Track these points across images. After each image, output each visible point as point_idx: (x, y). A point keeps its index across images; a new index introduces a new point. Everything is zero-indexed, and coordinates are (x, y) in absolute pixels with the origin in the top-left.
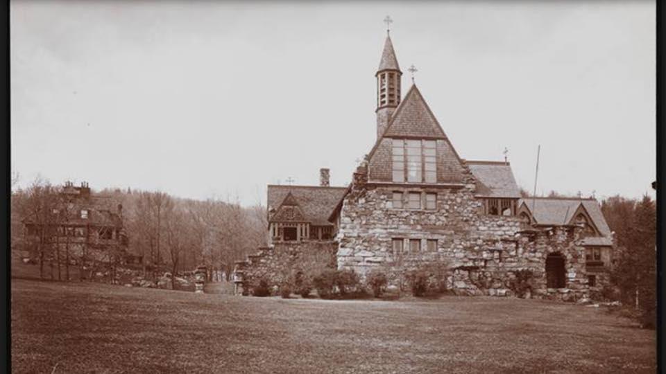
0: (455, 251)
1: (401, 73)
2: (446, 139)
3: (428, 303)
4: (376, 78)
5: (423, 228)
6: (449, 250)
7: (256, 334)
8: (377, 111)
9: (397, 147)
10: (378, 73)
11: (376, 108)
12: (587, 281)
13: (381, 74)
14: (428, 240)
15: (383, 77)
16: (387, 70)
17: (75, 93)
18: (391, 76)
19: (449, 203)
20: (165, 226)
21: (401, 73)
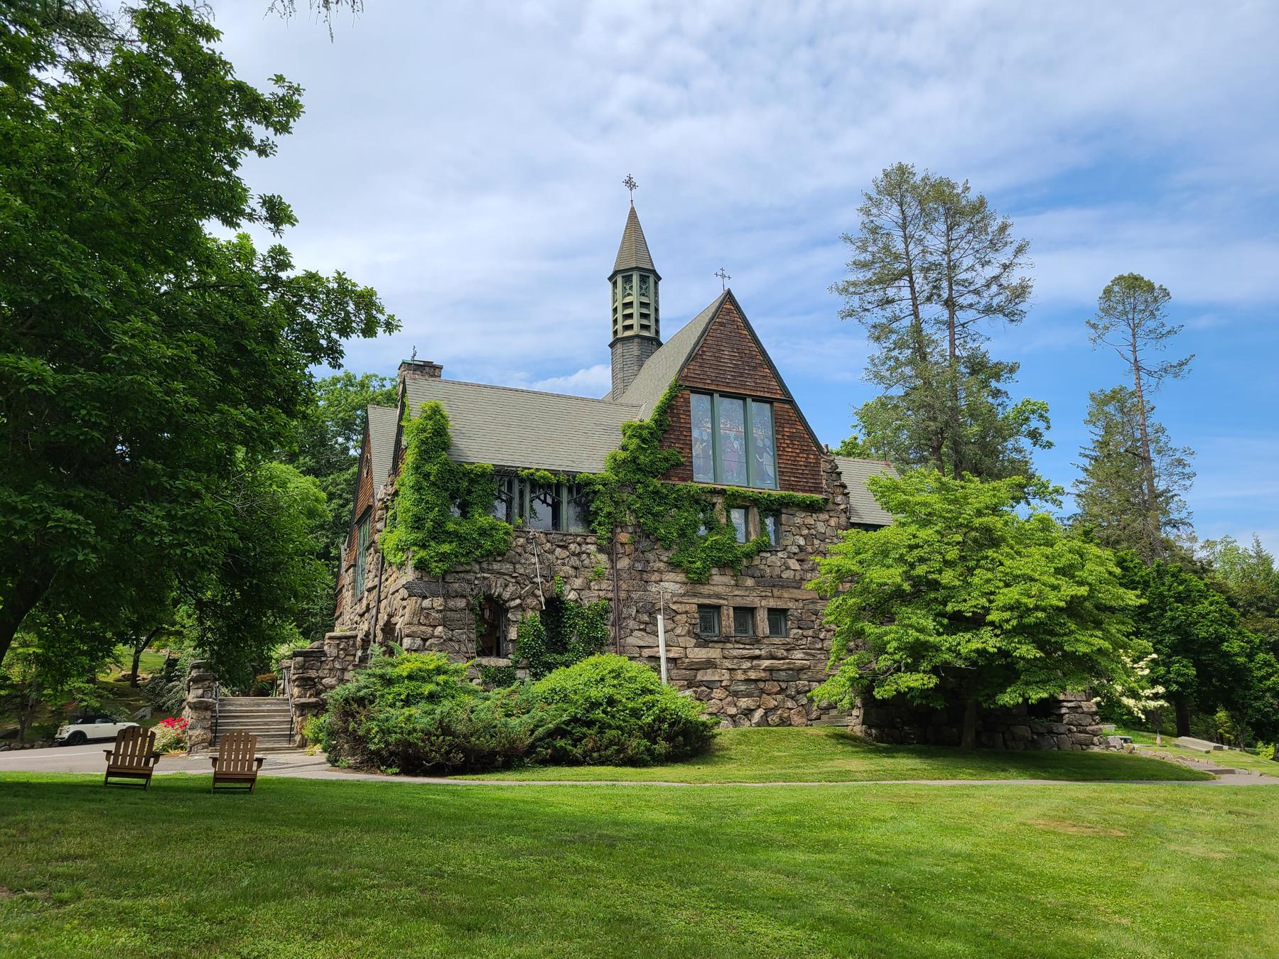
0: (822, 636)
1: (660, 279)
2: (790, 401)
3: (980, 783)
4: (610, 285)
5: (758, 584)
6: (810, 633)
7: (513, 841)
8: (406, 365)
9: (698, 404)
10: (615, 273)
11: (611, 339)
12: (143, 675)
13: (621, 276)
14: (770, 610)
15: (615, 284)
16: (637, 268)
17: (630, 183)
18: (644, 279)
19: (805, 532)
20: (588, 540)
21: (660, 279)
